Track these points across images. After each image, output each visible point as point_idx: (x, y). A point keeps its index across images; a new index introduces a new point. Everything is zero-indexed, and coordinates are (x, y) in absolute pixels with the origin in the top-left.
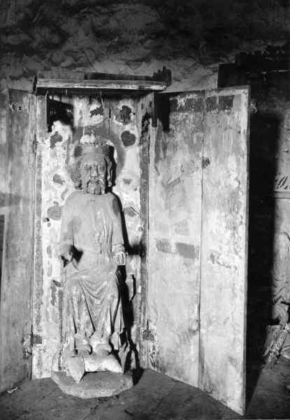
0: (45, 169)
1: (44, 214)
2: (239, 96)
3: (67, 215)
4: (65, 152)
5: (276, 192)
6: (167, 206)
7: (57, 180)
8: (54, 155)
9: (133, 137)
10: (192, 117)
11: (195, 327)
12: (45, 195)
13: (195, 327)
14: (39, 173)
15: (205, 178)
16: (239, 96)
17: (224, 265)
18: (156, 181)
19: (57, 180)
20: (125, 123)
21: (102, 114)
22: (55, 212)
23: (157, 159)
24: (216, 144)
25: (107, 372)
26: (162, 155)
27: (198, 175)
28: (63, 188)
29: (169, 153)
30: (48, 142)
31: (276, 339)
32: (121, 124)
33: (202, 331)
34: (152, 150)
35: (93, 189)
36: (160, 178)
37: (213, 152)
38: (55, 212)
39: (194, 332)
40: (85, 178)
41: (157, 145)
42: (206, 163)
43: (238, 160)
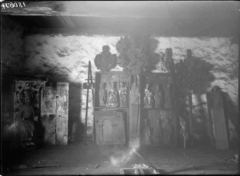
0: (15, 100)
1: (14, 110)
2: (67, 84)
3: (21, 111)
4: (20, 95)
5: (232, 42)
6: (47, 107)
7: (18, 102)
8: (17, 96)
9: (37, 92)
10: (235, 161)
11: (54, 132)
12: (14, 106)
13: (54, 132)
14: (13, 101)
15: (57, 100)
16: (67, 84)
17: (63, 117)
18: (43, 101)
19: (18, 102)
20: (35, 89)
21: (29, 86)
22: (17, 110)
23: (43, 97)
24: (60, 93)
25: (32, 145)
26: (45, 95)
27: (55, 100)
28: (19, 104)
29: (47, 95)
30: (15, 94)
31: (61, 172)
32: (34, 89)
33: (57, 132)
34: (42, 95)
35: (28, 104)
36: (44, 101)
37: (59, 95)
38: (17, 110)
39: (53, 133)
40: (26, 101)
41: (43, 93)
42: (57, 97)
43: (66, 96)
